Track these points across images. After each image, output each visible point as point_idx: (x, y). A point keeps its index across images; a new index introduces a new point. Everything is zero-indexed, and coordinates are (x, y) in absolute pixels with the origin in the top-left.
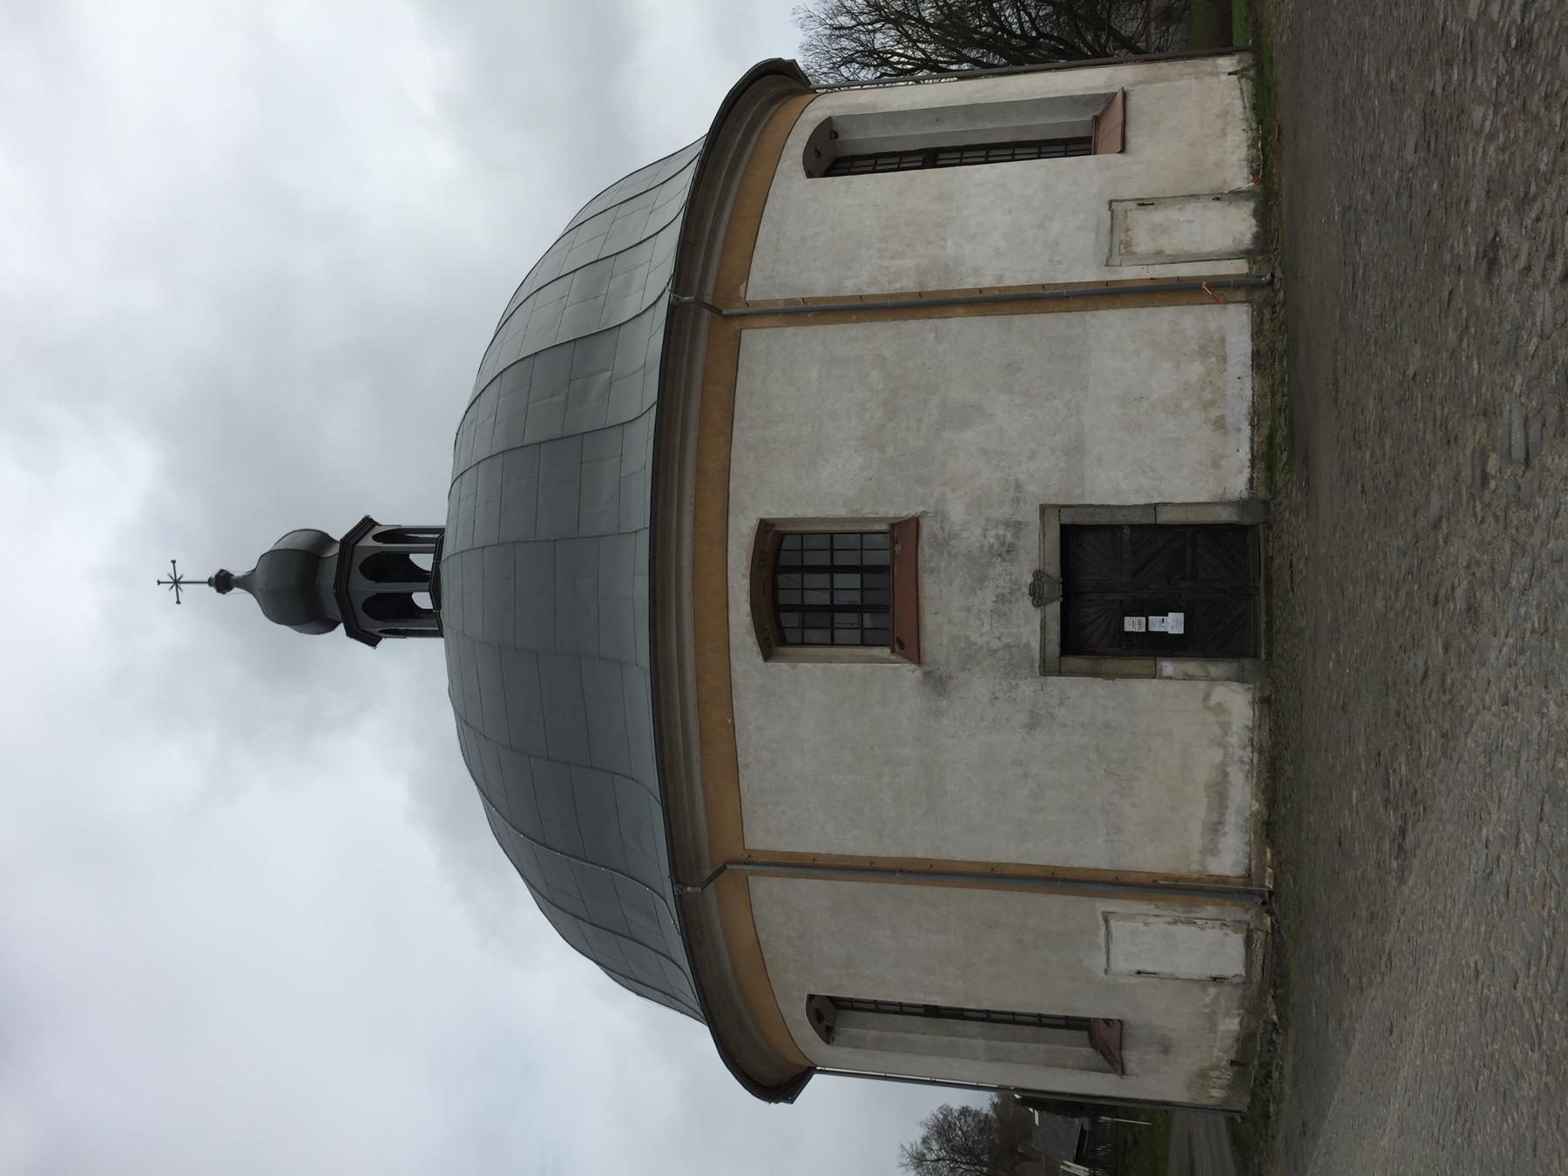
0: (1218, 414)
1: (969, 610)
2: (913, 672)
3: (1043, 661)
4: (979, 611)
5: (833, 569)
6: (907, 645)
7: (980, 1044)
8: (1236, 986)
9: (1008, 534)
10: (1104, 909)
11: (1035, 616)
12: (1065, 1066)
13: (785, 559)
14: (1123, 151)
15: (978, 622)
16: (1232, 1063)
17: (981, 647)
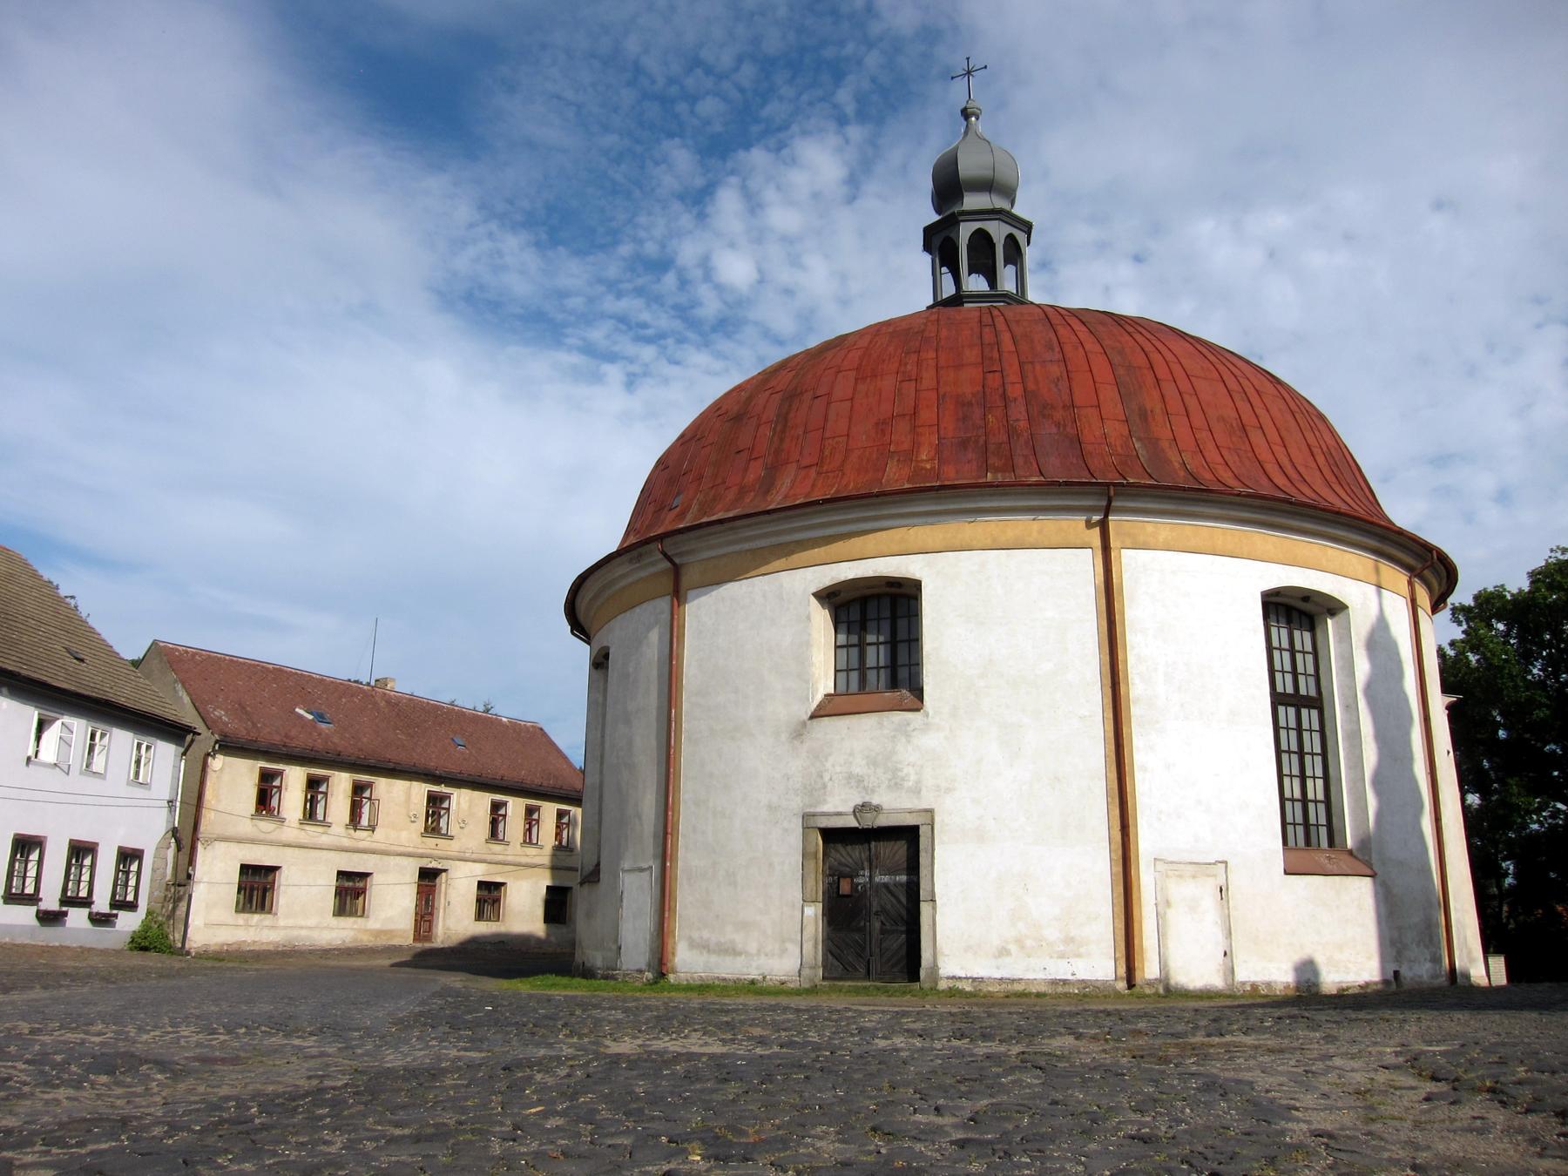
3: (814, 815)
11: (849, 808)
17: (824, 766)
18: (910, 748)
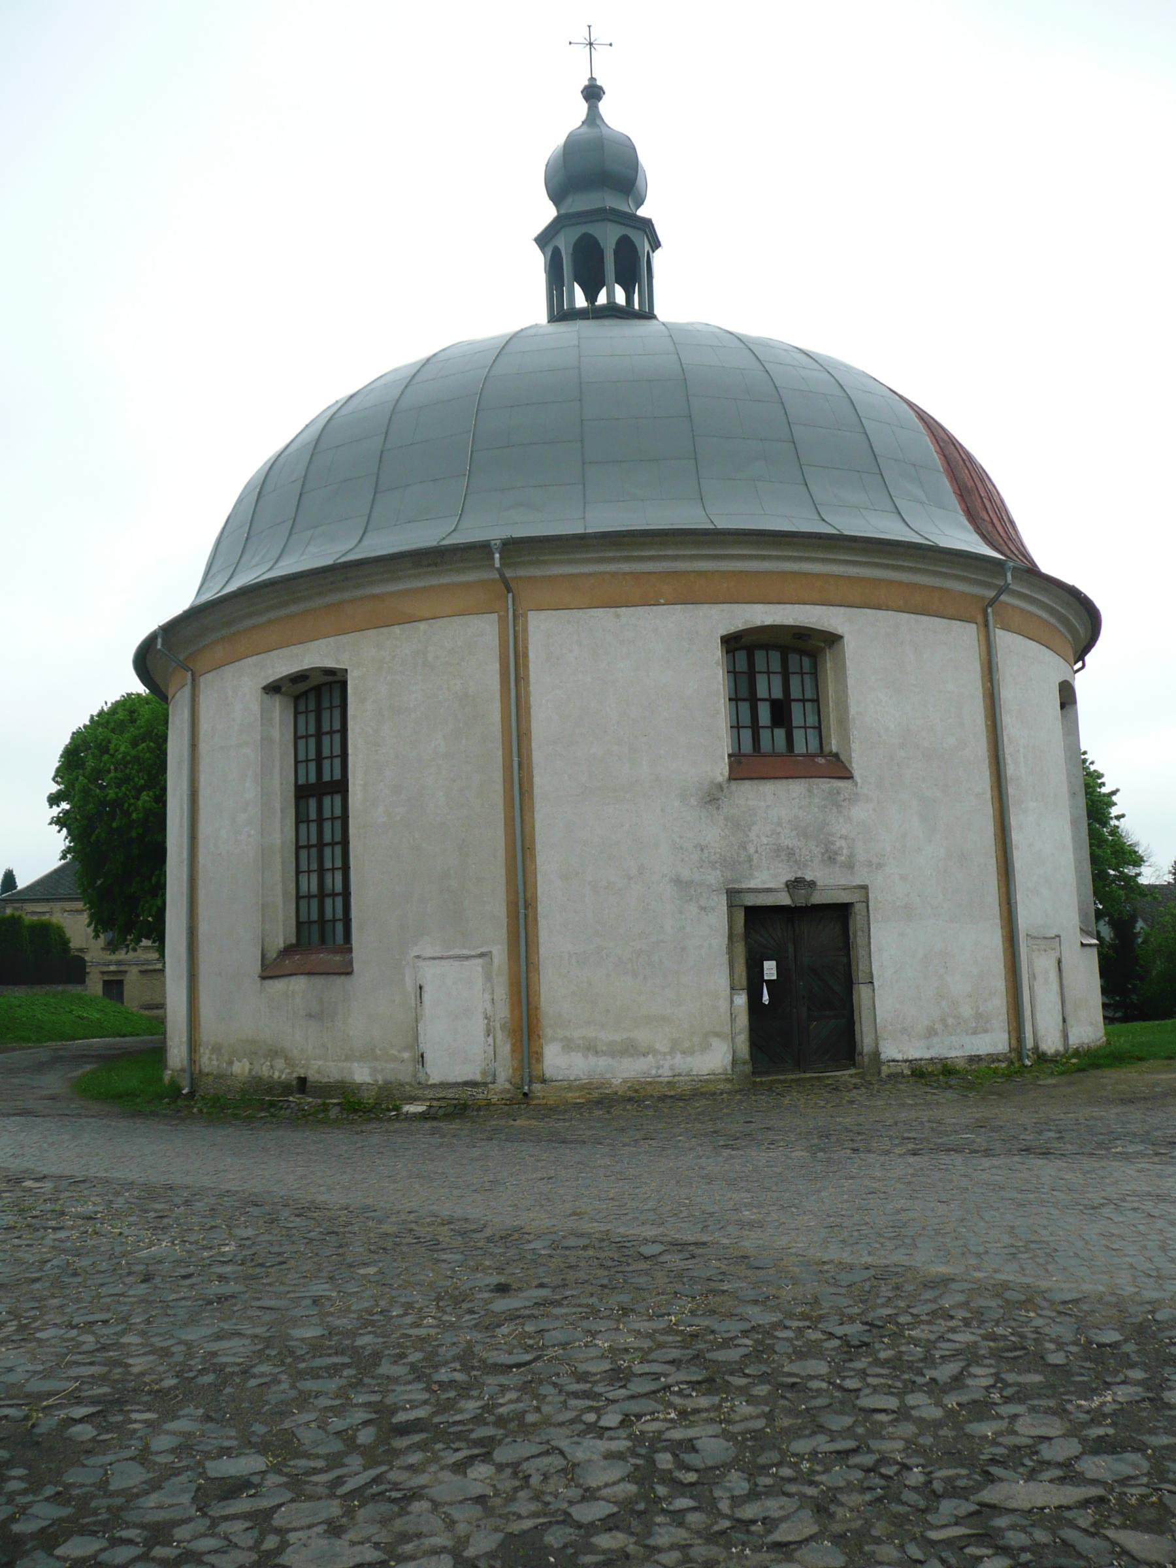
1: (779, 824)
3: (739, 891)
4: (779, 833)
8: (415, 1076)
9: (843, 858)
10: (495, 952)
11: (779, 882)
12: (263, 922)
13: (793, 659)
15: (769, 833)
17: (748, 836)
18: (841, 820)
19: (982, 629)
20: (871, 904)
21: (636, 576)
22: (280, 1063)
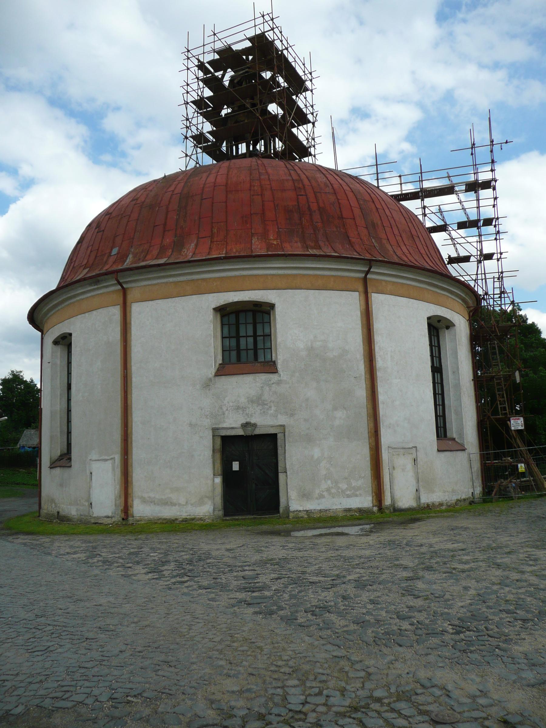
0: (325, 496)
2: (211, 374)
3: (218, 429)
5: (255, 336)
6: (221, 371)
7: (58, 408)
9: (272, 412)
10: (116, 458)
11: (238, 424)
14: (438, 451)
16: (58, 512)
19: (363, 296)
20: (286, 434)
21: (175, 283)
22: (53, 505)
